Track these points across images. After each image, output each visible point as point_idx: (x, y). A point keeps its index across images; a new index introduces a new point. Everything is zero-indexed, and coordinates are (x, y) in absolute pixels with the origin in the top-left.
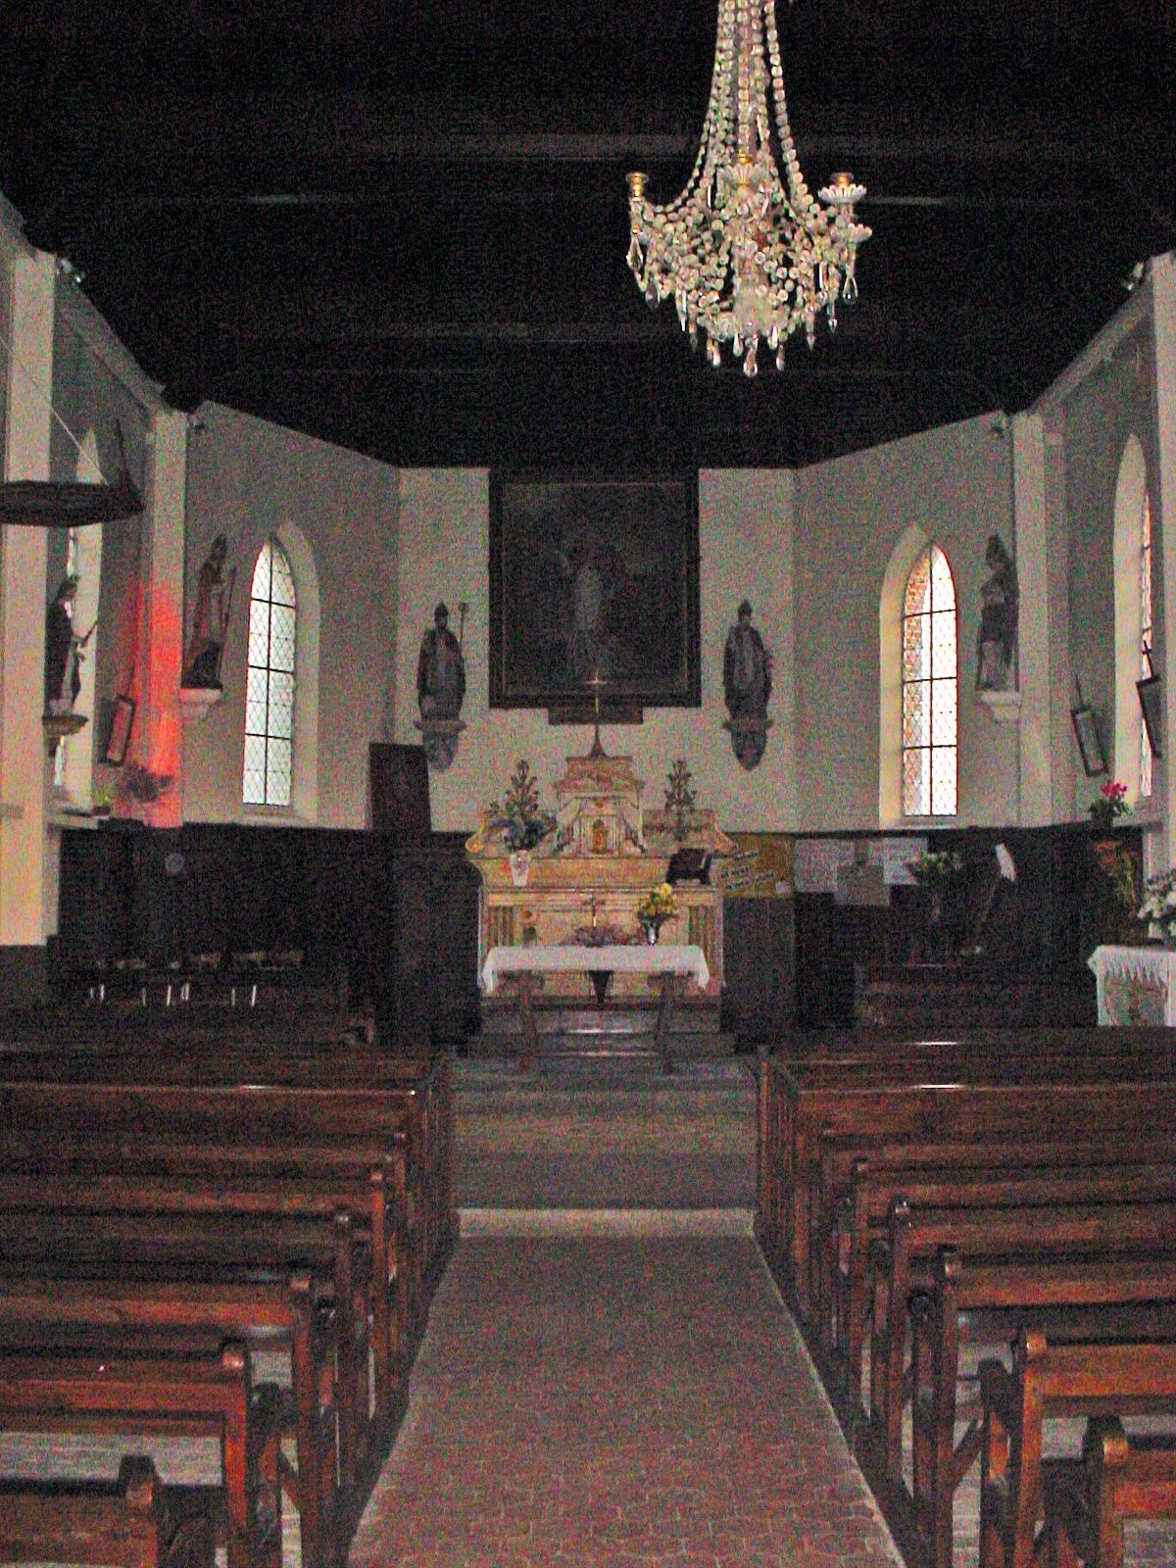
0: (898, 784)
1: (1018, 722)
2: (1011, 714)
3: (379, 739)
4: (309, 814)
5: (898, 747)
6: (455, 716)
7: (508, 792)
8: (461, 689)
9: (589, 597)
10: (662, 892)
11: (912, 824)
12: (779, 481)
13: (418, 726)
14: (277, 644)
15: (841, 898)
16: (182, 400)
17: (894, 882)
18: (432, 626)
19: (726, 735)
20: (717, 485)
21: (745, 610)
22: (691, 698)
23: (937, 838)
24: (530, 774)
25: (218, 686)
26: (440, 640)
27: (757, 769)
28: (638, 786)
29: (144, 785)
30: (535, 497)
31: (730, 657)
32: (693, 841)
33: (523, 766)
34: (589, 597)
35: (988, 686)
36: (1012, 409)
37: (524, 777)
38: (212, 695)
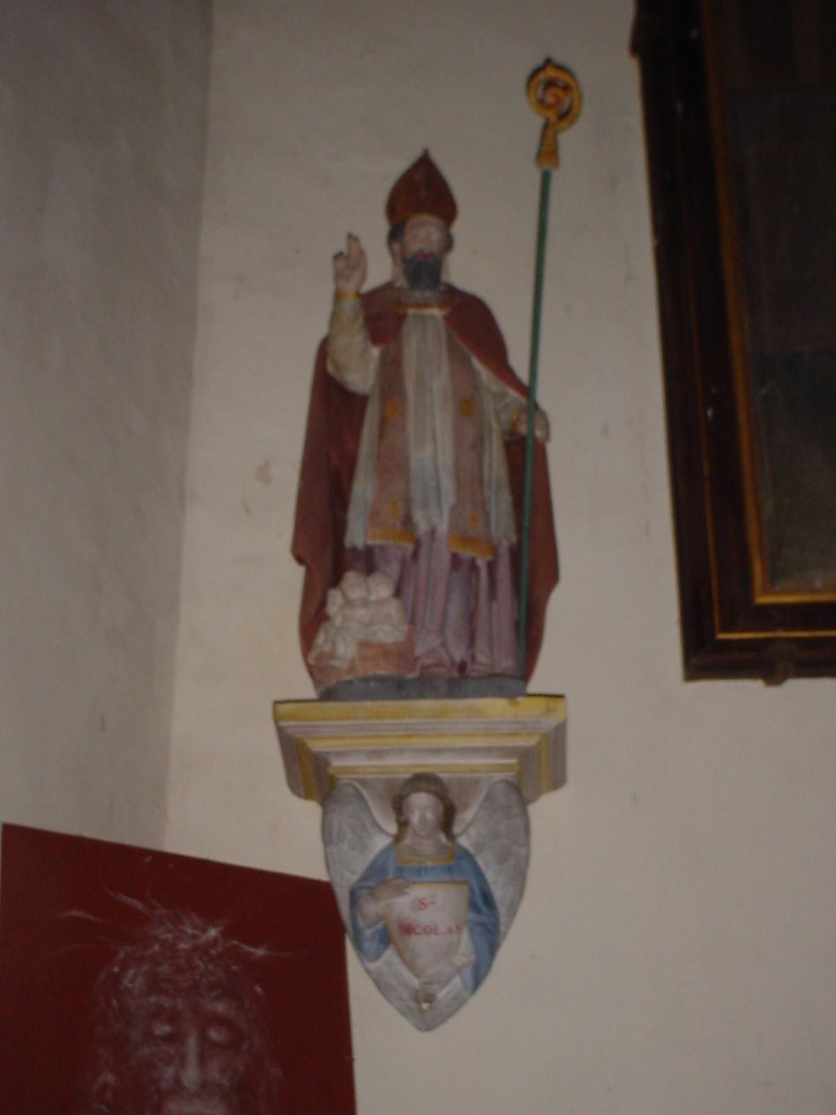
8: (532, 566)
18: (380, 269)
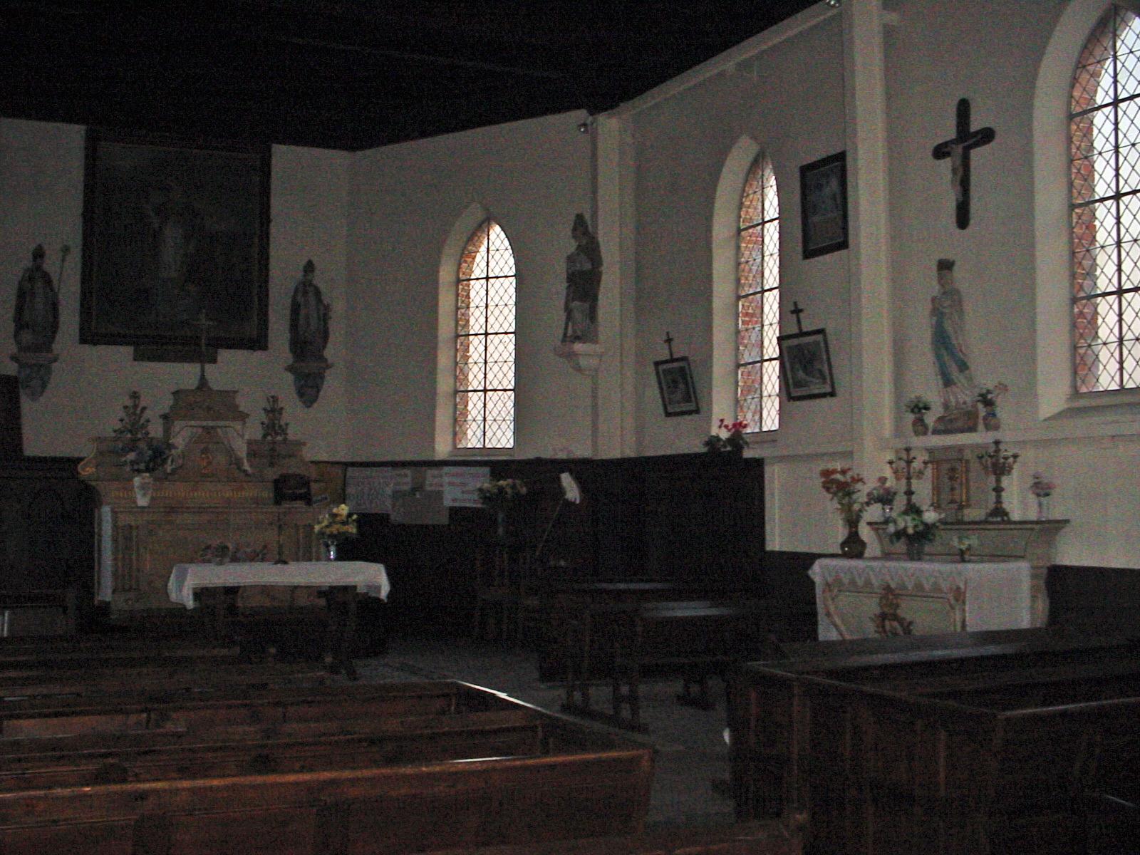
0: (451, 421)
1: (596, 370)
2: (594, 362)
5: (451, 391)
6: (49, 350)
7: (121, 420)
8: (55, 327)
9: (173, 248)
10: (341, 512)
11: (488, 455)
12: (338, 158)
15: (396, 518)
17: (451, 504)
19: (289, 377)
20: (287, 160)
21: (309, 267)
22: (258, 342)
23: (497, 465)
24: (143, 404)
26: (35, 282)
27: (315, 405)
28: (243, 417)
30: (126, 157)
31: (295, 309)
32: (292, 467)
33: (135, 396)
34: (173, 248)
35: (577, 338)
36: (595, 110)
37: (136, 406)
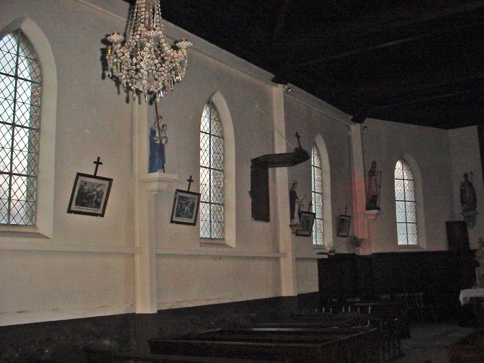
3: (450, 220)
4: (424, 247)
13: (461, 214)
14: (408, 193)
16: (358, 119)
25: (379, 209)
29: (356, 242)
38: (375, 212)
